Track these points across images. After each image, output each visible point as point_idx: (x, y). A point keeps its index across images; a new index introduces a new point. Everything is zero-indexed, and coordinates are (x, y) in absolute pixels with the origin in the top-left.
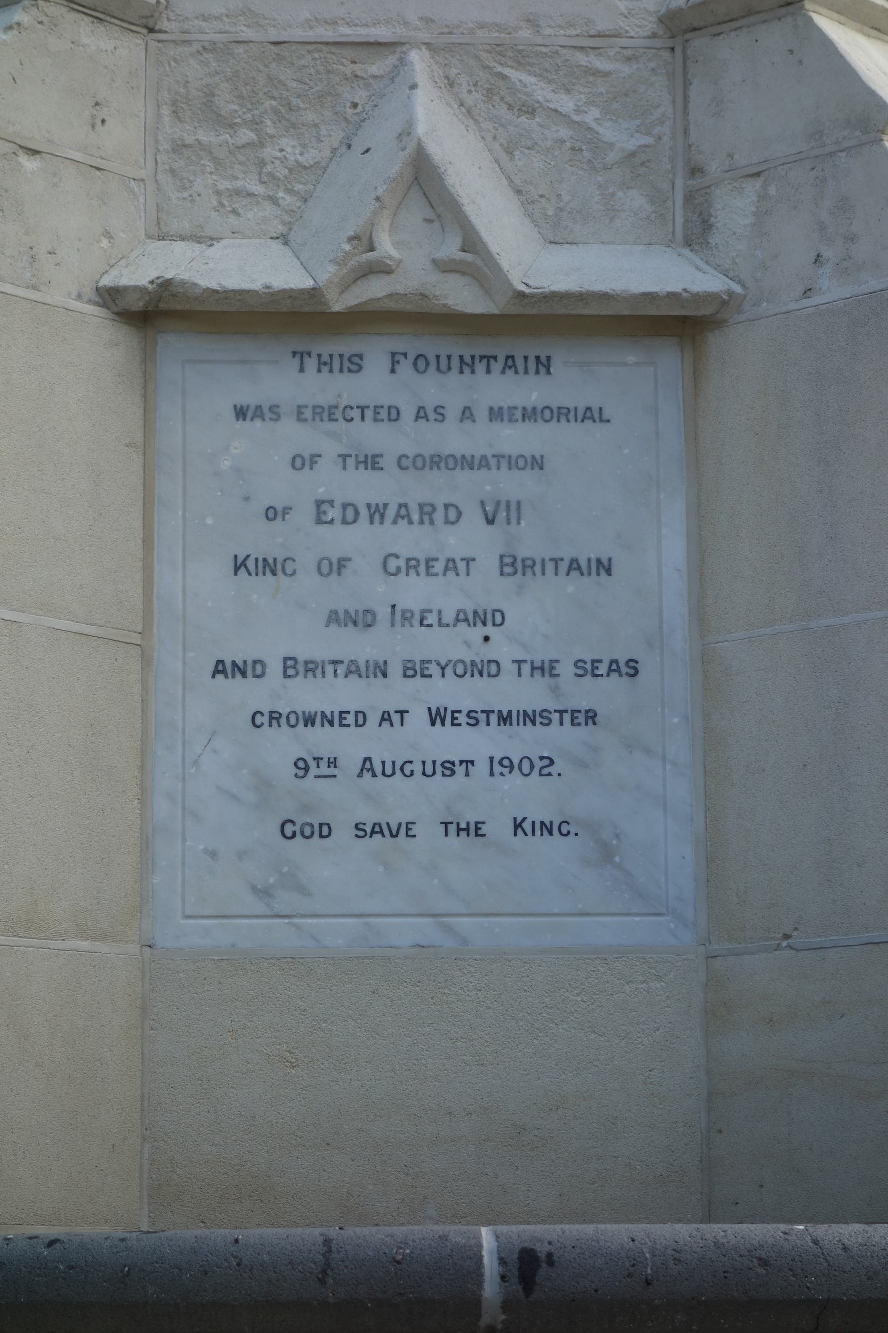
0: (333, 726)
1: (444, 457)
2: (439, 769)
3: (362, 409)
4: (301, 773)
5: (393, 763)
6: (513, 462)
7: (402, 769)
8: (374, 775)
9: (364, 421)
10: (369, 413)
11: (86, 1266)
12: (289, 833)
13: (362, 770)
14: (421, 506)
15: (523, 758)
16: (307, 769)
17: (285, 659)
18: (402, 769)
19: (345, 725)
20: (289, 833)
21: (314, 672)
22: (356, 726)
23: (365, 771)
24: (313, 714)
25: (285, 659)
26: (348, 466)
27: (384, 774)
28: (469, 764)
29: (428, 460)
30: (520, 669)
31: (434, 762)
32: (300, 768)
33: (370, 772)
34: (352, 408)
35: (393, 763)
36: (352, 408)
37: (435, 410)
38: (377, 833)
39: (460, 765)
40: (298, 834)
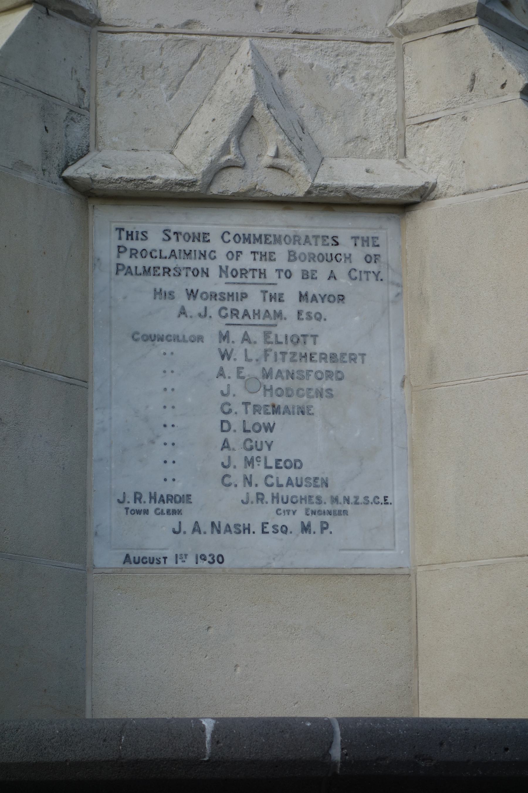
5: (331, 254)
35: (331, 254)
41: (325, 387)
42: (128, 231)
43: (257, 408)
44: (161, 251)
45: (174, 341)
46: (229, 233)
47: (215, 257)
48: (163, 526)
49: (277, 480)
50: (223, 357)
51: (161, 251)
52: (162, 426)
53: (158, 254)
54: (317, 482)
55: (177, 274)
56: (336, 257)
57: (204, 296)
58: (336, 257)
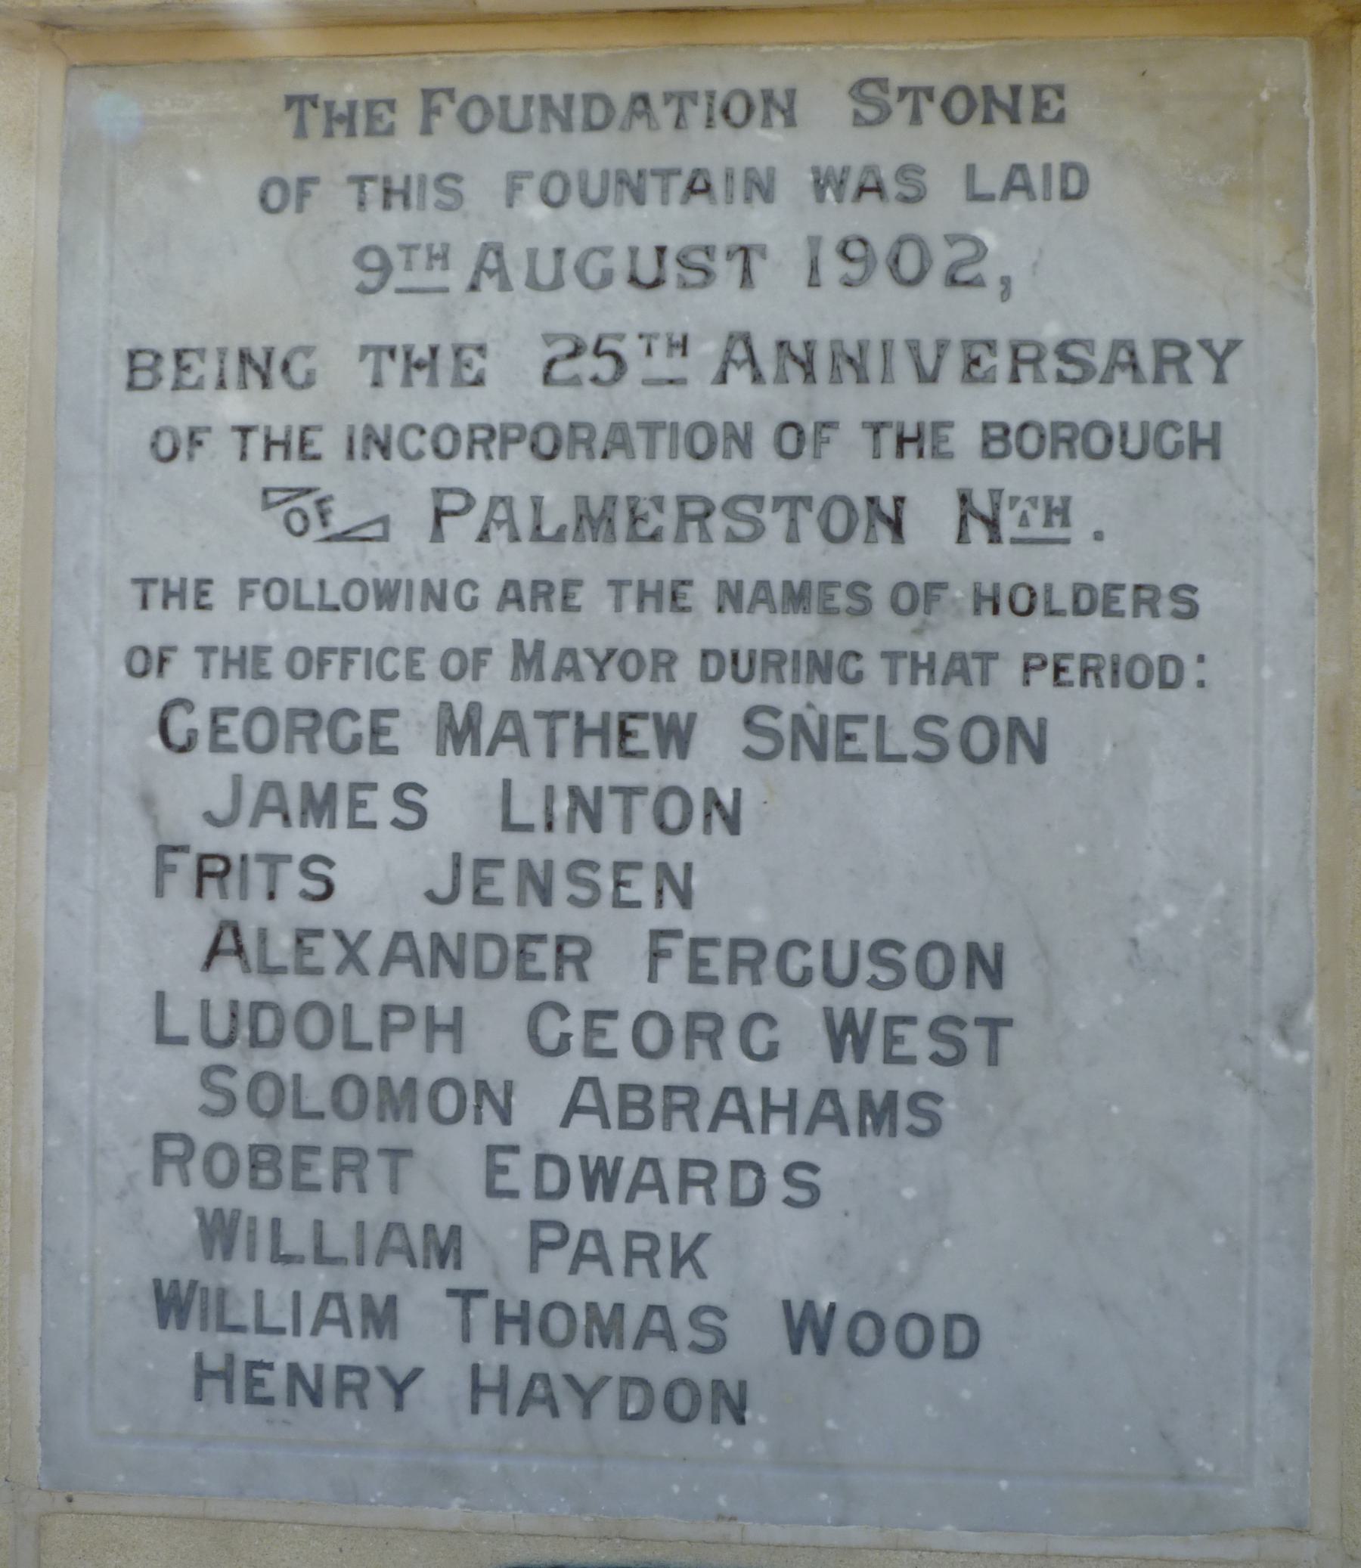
0: (521, 861)
1: (326, 714)
2: (671, 268)
4: (372, 280)
7: (580, 270)
11: (597, 1552)
12: (550, 1038)
13: (477, 273)
14: (1159, 345)
16: (386, 268)
17: (160, 1139)
18: (580, 270)
20: (550, 1038)
23: (484, 274)
25: (160, 1139)
27: (533, 283)
29: (679, 1029)
31: (661, 250)
32: (369, 270)
37: (788, 1174)
40: (577, 1041)
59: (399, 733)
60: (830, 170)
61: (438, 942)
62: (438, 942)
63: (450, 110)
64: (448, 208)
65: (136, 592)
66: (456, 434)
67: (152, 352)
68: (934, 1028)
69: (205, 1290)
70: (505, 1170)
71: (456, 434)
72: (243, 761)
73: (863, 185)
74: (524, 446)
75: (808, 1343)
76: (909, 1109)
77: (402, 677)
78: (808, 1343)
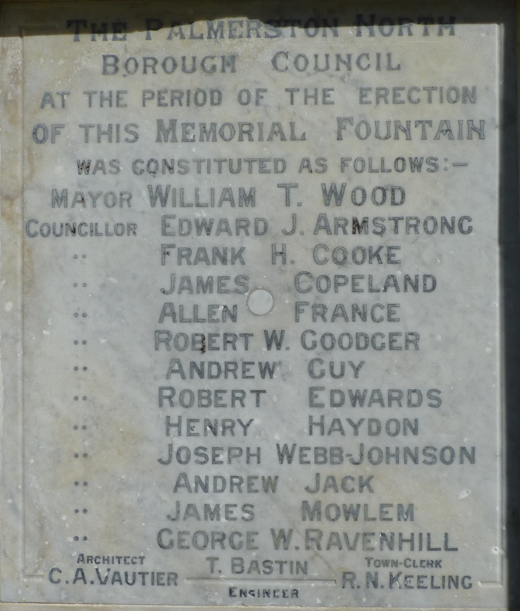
3: (119, 558)
5: (194, 58)
6: (52, 231)
7: (358, 64)
8: (283, 139)
9: (125, 572)
10: (122, 561)
15: (365, 139)
19: (247, 377)
21: (323, 455)
22: (243, 378)
24: (362, 392)
26: (93, 104)
28: (427, 125)
30: (87, 135)
33: (279, 135)
34: (136, 558)
35: (194, 58)
36: (136, 558)
38: (80, 579)
39: (304, 134)
41: (115, 89)
42: (171, 106)
43: (348, 576)
44: (432, 577)
45: (91, 235)
46: (286, 55)
47: (470, 230)
48: (71, 556)
49: (220, 390)
50: (281, 456)
51: (432, 577)
52: (88, 537)
53: (411, 563)
54: (215, 313)
55: (131, 137)
56: (202, 65)
57: (393, 427)
58: (202, 65)
59: (258, 540)
60: (204, 220)
61: (355, 308)
62: (355, 308)
63: (351, 129)
64: (432, 171)
65: (366, 561)
66: (222, 136)
67: (113, 56)
68: (237, 280)
69: (174, 190)
70: (387, 512)
71: (222, 136)
72: (313, 468)
73: (280, 366)
74: (155, 101)
75: (274, 346)
76: (326, 450)
77: (245, 547)
78: (274, 346)
